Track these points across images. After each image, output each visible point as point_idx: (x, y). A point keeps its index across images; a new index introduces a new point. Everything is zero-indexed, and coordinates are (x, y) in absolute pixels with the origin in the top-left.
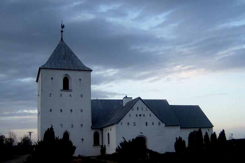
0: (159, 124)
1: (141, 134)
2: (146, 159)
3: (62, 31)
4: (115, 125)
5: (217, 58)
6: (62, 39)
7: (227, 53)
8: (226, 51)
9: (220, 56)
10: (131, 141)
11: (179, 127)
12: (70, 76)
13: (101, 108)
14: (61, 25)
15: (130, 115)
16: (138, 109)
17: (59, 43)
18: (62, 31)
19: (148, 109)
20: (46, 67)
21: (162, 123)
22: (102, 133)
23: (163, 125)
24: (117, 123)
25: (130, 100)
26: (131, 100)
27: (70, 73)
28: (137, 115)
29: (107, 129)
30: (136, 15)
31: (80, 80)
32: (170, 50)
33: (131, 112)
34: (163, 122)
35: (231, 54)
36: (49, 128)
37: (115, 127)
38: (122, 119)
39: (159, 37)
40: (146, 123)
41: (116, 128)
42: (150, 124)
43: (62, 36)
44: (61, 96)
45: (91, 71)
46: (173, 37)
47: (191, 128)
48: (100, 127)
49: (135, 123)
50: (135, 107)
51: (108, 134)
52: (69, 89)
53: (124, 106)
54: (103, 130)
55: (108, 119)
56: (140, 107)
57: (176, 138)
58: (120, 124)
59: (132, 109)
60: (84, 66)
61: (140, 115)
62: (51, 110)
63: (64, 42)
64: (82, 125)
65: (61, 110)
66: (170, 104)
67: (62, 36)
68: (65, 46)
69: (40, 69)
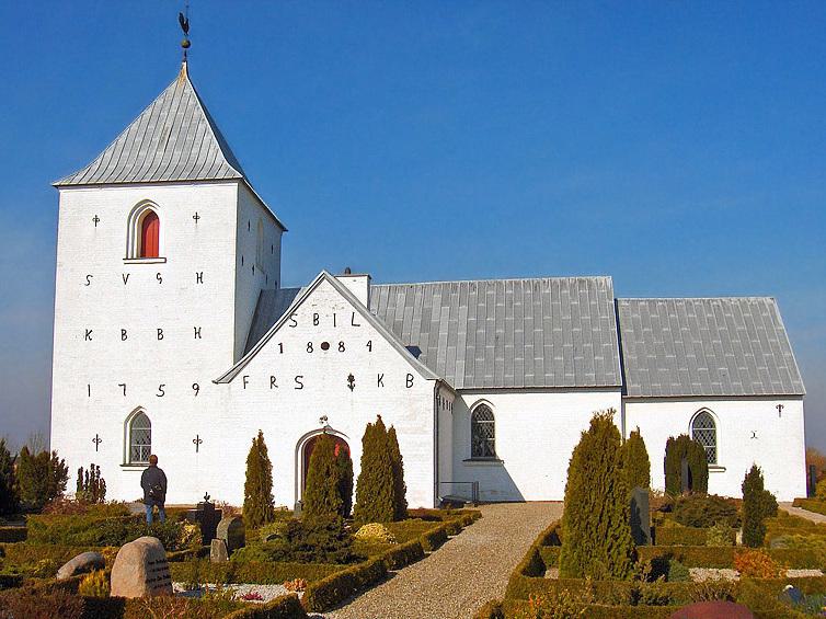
0: (409, 380)
15: (280, 344)
27: (714, 407)
28: (310, 346)
31: (197, 218)
40: (351, 378)
49: (161, 393)
56: (325, 314)
59: (290, 322)
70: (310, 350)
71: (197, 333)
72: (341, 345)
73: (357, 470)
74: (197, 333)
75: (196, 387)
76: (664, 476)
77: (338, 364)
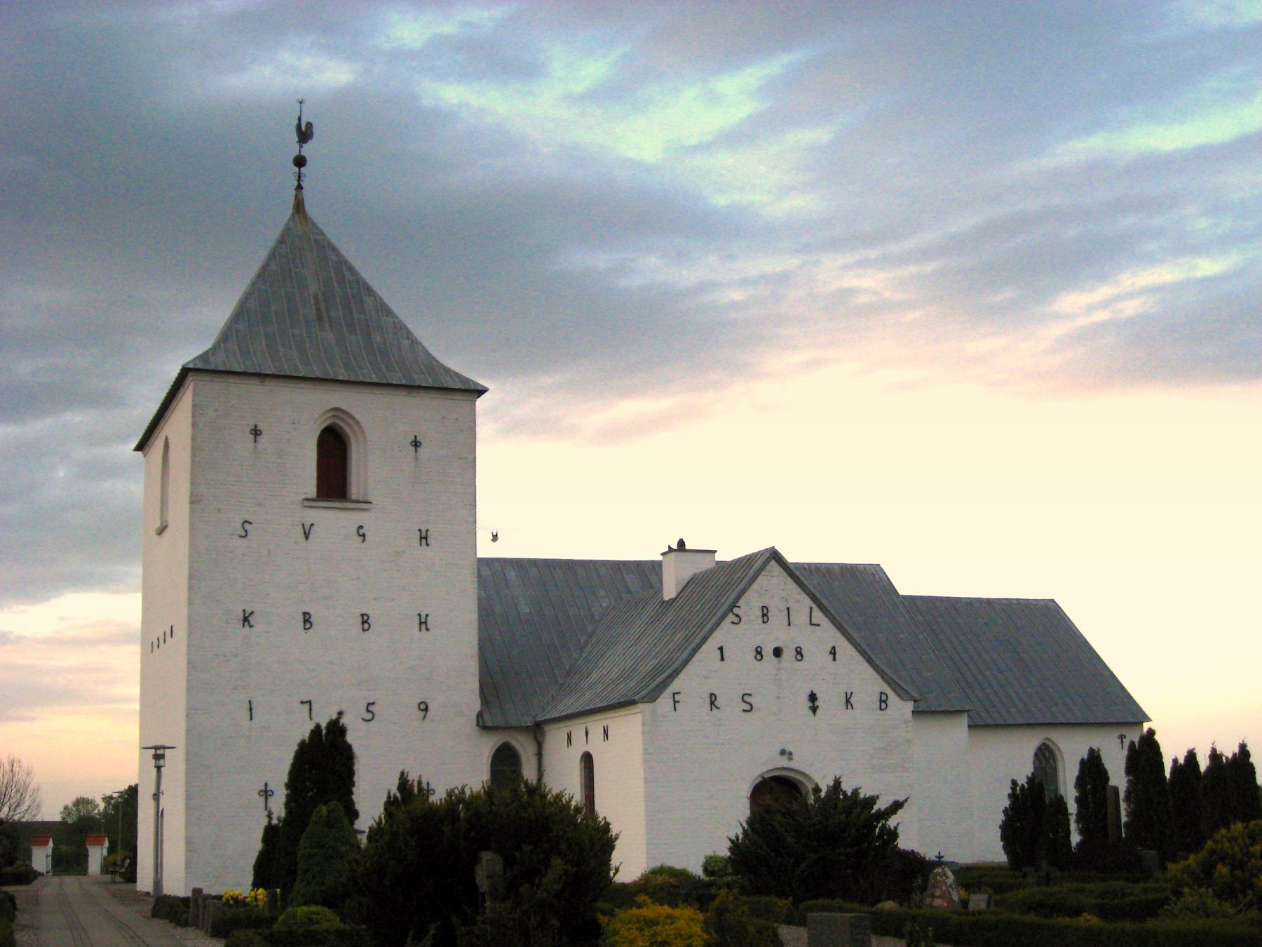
0: (883, 701)
1: (783, 762)
2: (937, 902)
3: (300, 162)
4: (641, 706)
5: (1056, 331)
6: (299, 206)
7: (1106, 304)
8: (1103, 292)
9: (1069, 317)
10: (1204, 763)
11: (964, 721)
12: (357, 422)
13: (525, 609)
14: (296, 122)
15: (721, 649)
16: (765, 616)
17: (287, 229)
18: (300, 162)
19: (818, 616)
20: (218, 363)
21: (897, 699)
22: (540, 755)
23: (901, 709)
24: (652, 697)
25: (704, 565)
26: (711, 565)
28: (759, 652)
29: (577, 728)
30: (594, 70)
31: (416, 444)
32: (783, 279)
33: (725, 634)
34: (903, 694)
35: (1130, 308)
36: (324, 725)
37: (639, 718)
38: (676, 673)
39: (721, 201)
40: (813, 697)
41: (644, 725)
42: (830, 700)
43: (299, 187)
44: (307, 538)
45: (481, 392)
46: (801, 204)
47: (1029, 725)
48: (528, 721)
49: (369, 716)
50: (750, 605)
51: (587, 760)
52: (354, 497)
53: (666, 598)
54: (543, 734)
55: (568, 675)
57: (1014, 783)
58: (665, 700)
59: (731, 617)
60: (433, 366)
61: (778, 652)
62: (246, 619)
63: (314, 224)
64: (424, 708)
65: (307, 620)
66: (906, 585)
67: (299, 187)
68: (325, 248)
69: (185, 372)
70: (759, 657)
71: (423, 623)
72: (799, 652)
73: (1072, 808)
74: (423, 623)
75: (423, 707)
76: (259, 846)
77: (800, 678)
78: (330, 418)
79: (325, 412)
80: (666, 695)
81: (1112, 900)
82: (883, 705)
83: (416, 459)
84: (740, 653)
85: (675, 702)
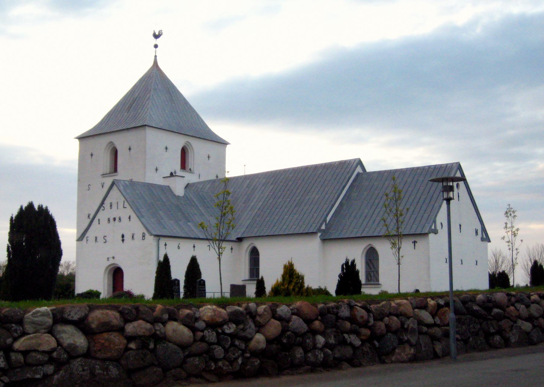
19: (126, 204)
31: (130, 149)
40: (123, 236)
61: (115, 219)
78: (110, 146)
79: (107, 145)
80: (85, 238)
81: (179, 353)
82: (144, 238)
83: (130, 154)
84: (104, 221)
85: (87, 240)
